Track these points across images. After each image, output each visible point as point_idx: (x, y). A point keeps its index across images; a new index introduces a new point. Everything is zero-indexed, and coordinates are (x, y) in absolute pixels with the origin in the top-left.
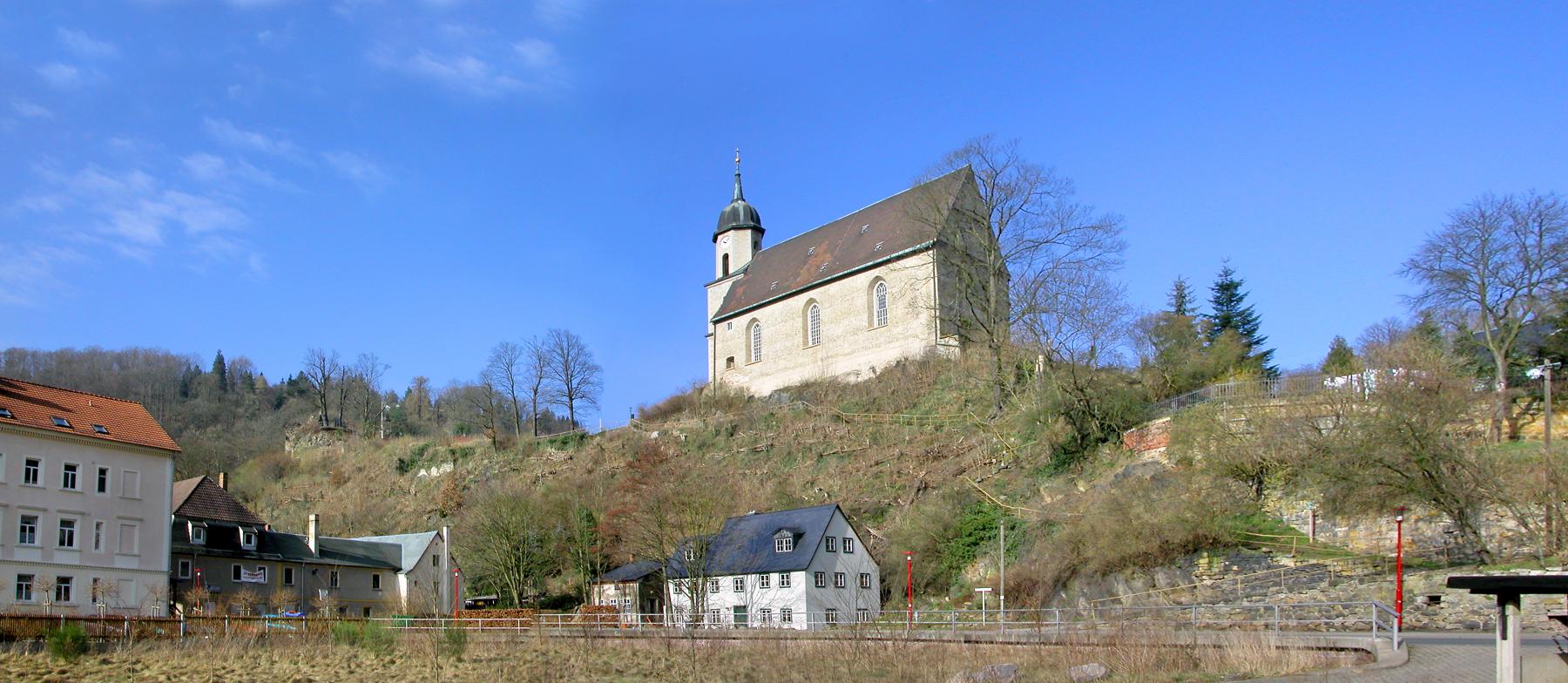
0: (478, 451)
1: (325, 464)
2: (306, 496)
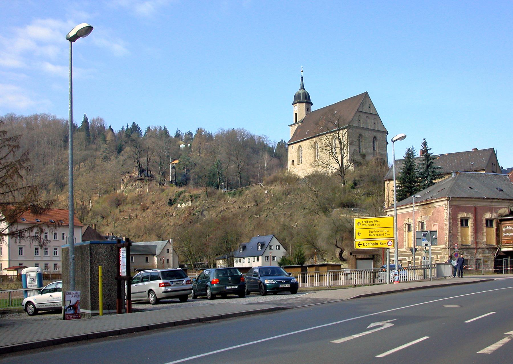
0: (202, 196)
1: (139, 198)
2: (130, 216)
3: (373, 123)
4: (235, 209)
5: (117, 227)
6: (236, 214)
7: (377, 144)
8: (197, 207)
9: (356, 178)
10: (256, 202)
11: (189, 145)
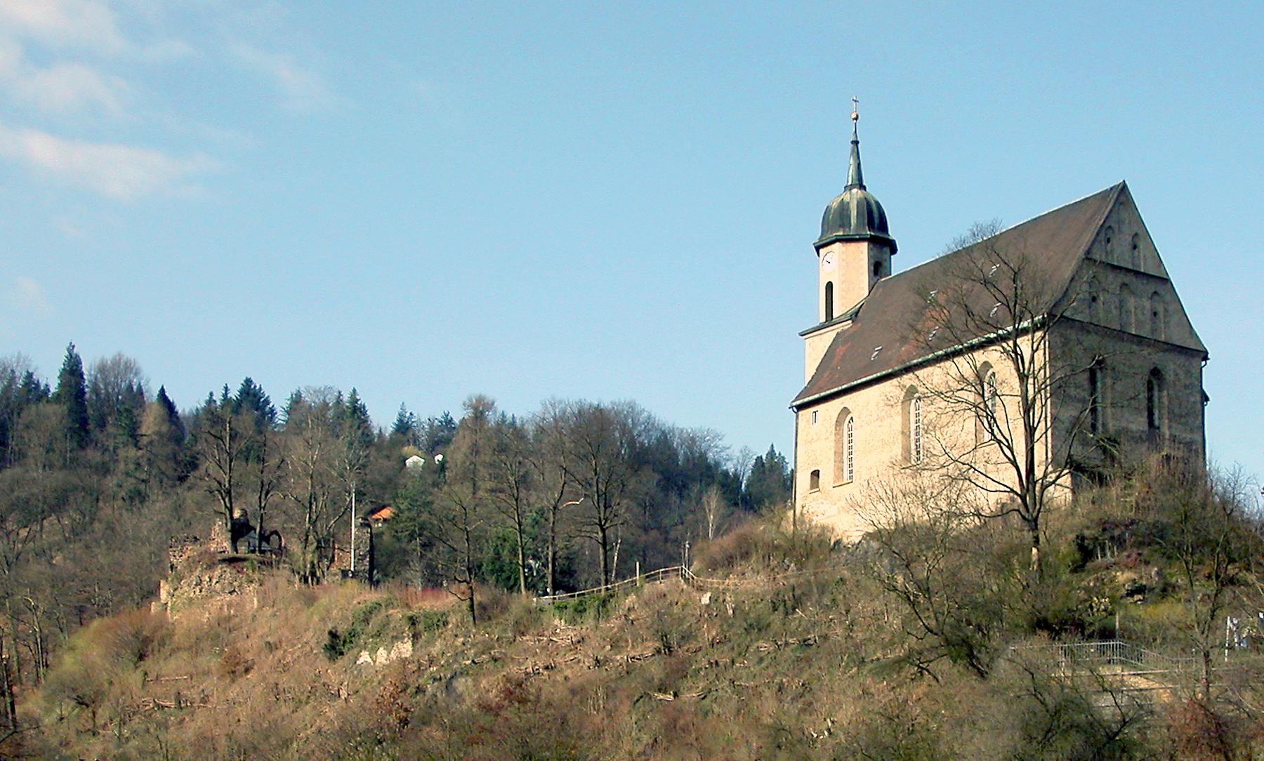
0: (453, 620)
1: (220, 633)
3: (1148, 315)
4: (577, 669)
5: (128, 739)
6: (583, 689)
7: (1163, 397)
8: (431, 662)
9: (1087, 533)
10: (664, 637)
11: (440, 457)
